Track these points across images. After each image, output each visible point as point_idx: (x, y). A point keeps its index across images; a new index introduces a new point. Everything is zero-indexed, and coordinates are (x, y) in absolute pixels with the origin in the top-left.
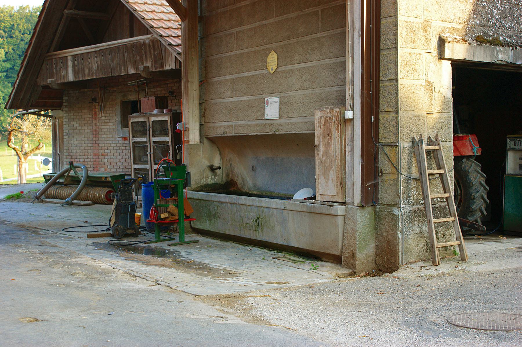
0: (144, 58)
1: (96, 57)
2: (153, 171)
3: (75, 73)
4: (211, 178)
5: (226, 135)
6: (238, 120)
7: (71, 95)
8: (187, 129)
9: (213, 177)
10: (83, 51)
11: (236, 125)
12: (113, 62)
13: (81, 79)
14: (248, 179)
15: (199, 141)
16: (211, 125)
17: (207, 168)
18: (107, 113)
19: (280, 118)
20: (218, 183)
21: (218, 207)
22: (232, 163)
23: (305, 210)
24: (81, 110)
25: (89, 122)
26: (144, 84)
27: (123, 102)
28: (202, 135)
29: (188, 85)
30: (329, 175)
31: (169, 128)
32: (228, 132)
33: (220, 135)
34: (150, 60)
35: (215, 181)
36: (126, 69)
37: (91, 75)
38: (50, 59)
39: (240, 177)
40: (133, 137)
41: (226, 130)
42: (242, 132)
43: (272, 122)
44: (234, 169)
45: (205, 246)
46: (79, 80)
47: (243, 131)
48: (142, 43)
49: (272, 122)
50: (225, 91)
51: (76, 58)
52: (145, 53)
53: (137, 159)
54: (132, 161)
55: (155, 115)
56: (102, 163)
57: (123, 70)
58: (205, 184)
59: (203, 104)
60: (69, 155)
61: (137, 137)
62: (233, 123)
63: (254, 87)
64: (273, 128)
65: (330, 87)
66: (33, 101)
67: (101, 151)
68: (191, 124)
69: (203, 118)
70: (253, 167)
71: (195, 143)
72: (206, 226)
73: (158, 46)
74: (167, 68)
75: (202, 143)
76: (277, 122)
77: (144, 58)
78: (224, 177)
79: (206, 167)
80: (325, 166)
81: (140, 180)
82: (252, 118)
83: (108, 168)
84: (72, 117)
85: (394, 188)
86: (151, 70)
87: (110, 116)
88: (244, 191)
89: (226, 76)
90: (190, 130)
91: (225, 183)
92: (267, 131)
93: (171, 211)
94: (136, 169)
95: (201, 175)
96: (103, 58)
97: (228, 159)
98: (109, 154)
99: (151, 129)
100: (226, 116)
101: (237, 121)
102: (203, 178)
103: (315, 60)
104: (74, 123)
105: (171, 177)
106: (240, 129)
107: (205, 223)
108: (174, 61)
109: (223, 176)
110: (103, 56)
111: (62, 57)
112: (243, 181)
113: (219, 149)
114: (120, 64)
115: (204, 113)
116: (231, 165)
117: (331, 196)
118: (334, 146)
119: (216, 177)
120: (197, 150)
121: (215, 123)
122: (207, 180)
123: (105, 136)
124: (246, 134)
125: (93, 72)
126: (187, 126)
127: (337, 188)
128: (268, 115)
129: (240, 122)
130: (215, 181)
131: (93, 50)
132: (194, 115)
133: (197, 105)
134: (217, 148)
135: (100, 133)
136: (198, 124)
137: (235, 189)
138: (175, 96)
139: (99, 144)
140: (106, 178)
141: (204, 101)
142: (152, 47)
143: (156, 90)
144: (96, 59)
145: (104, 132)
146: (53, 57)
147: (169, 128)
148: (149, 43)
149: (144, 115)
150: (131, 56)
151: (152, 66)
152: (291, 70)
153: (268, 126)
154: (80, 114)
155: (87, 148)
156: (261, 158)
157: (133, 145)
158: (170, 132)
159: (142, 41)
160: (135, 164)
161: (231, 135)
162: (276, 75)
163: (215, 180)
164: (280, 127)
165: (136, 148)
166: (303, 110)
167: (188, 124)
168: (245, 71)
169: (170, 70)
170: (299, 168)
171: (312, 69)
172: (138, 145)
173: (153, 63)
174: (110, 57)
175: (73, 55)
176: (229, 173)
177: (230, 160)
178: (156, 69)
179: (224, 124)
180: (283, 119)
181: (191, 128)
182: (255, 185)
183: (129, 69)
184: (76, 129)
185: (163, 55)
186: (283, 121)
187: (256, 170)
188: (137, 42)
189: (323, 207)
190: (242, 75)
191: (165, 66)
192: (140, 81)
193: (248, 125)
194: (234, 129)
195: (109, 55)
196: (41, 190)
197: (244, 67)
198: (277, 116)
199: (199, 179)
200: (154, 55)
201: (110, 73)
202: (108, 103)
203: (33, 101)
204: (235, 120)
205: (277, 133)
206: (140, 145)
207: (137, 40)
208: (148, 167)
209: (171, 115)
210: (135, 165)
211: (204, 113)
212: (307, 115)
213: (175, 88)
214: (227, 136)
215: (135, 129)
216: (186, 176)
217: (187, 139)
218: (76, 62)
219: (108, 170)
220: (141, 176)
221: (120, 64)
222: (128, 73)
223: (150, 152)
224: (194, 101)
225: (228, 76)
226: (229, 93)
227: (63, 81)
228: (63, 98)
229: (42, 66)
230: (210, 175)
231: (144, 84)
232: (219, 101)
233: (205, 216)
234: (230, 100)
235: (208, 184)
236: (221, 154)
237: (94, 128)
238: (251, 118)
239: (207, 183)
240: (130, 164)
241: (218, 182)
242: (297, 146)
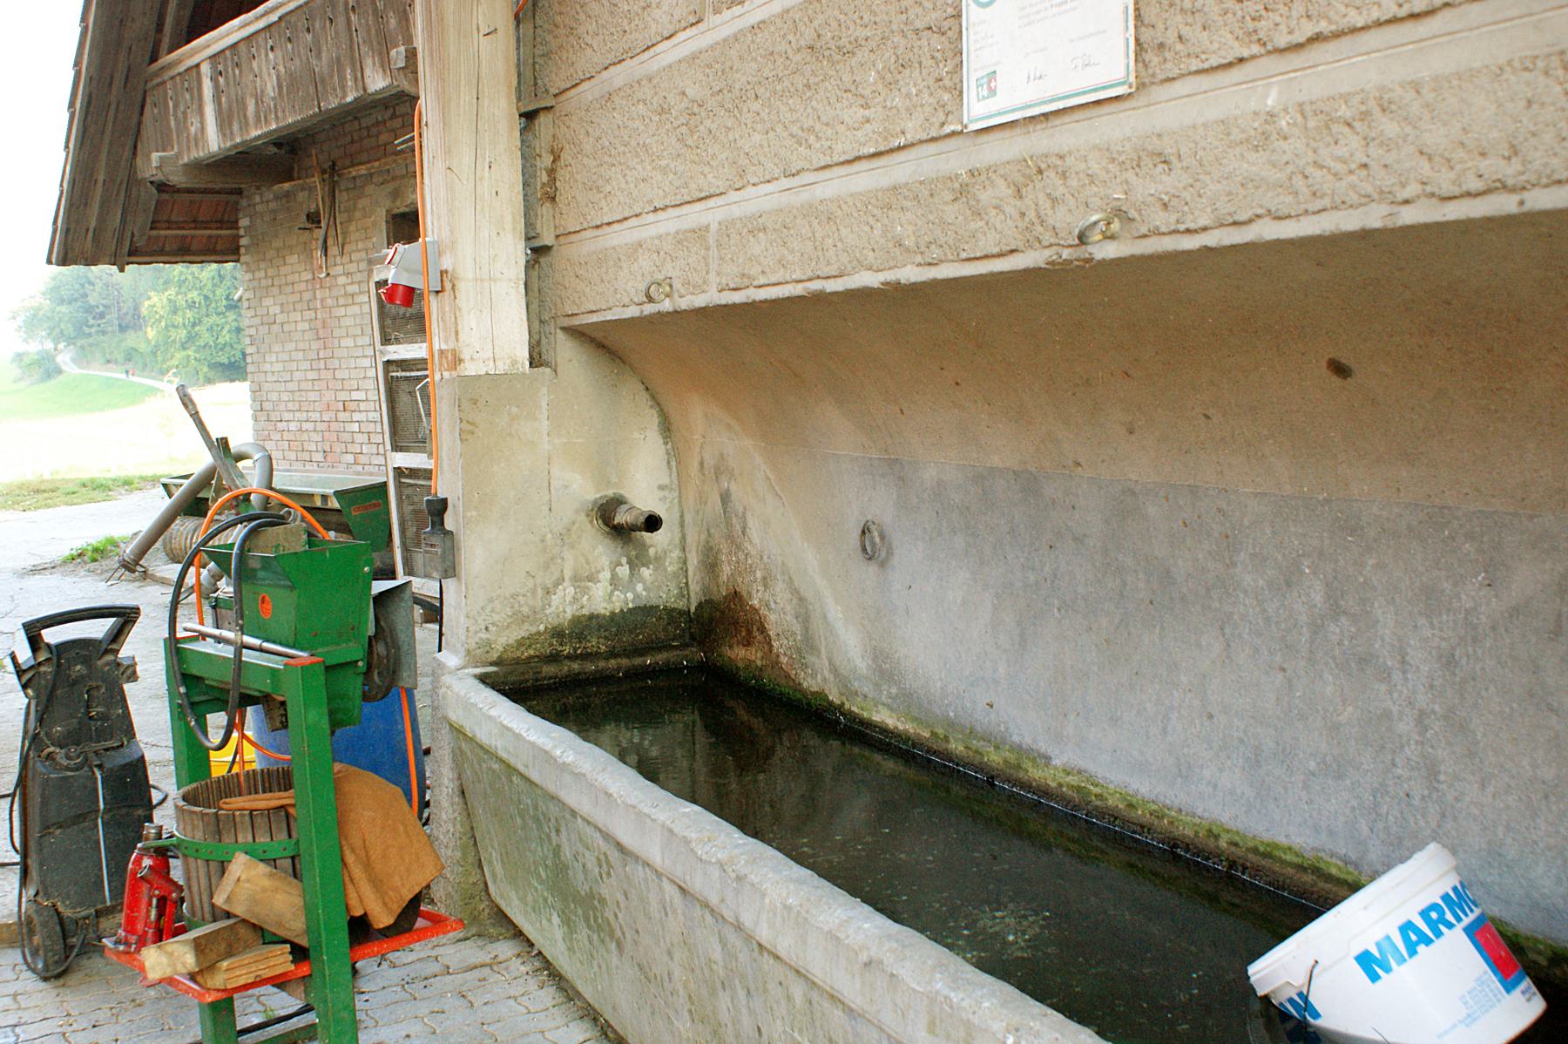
1: (272, 49)
3: (224, 122)
4: (615, 580)
5: (667, 306)
7: (258, 208)
8: (446, 283)
9: (624, 571)
10: (234, 35)
11: (726, 227)
12: (319, 56)
13: (238, 140)
14: (835, 613)
15: (523, 354)
16: (588, 245)
17: (582, 517)
18: (351, 261)
19: (1141, 86)
20: (654, 608)
22: (733, 487)
24: (284, 257)
25: (307, 296)
27: (395, 217)
32: (677, 285)
33: (632, 312)
35: (637, 596)
36: (360, 79)
37: (263, 119)
38: (158, 85)
39: (780, 587)
40: (386, 340)
41: (670, 270)
44: (744, 533)
46: (233, 143)
47: (782, 262)
51: (220, 67)
56: (347, 437)
57: (349, 83)
58: (576, 620)
60: (262, 410)
61: (398, 341)
64: (1054, 201)
66: (133, 234)
67: (343, 396)
69: (545, 210)
70: (865, 531)
71: (501, 368)
75: (547, 365)
76: (1116, 128)
78: (690, 573)
79: (577, 512)
82: (844, 149)
83: (361, 453)
84: (262, 281)
87: (360, 271)
90: (462, 287)
91: (700, 606)
94: (399, 468)
95: (546, 567)
96: (289, 46)
97: (710, 462)
98: (363, 406)
100: (664, 171)
101: (733, 196)
102: (560, 581)
104: (268, 302)
106: (757, 249)
109: (685, 562)
110: (289, 40)
111: (186, 70)
112: (805, 618)
113: (653, 397)
114: (338, 59)
115: (552, 172)
116: (725, 498)
119: (646, 572)
120: (514, 410)
121: (607, 229)
122: (585, 591)
123: (349, 342)
124: (798, 290)
125: (269, 105)
126: (447, 263)
128: (1000, 83)
129: (758, 199)
130: (637, 596)
131: (261, 24)
133: (503, 126)
134: (645, 395)
135: (337, 333)
136: (515, 254)
139: (335, 369)
140: (324, 497)
144: (271, 55)
145: (347, 327)
146: (166, 77)
150: (370, 18)
153: (1004, 190)
154: (284, 270)
155: (304, 386)
156: (929, 474)
157: (386, 372)
160: (397, 448)
161: (700, 301)
163: (639, 588)
164: (1147, 187)
170: (1318, 598)
172: (404, 374)
174: (309, 37)
175: (214, 56)
176: (719, 551)
177: (718, 473)
180: (1179, 88)
182: (885, 668)
183: (368, 72)
184: (275, 323)
187: (890, 554)
194: (714, 252)
195: (308, 30)
196: (142, 534)
199: (534, 592)
201: (313, 100)
202: (352, 228)
203: (133, 234)
204: (721, 185)
205: (1106, 251)
206: (408, 374)
210: (399, 455)
211: (552, 172)
214: (677, 313)
216: (372, 610)
217: (451, 346)
218: (221, 80)
219: (363, 460)
221: (338, 59)
222: (365, 90)
224: (485, 102)
227: (196, 155)
228: (237, 222)
229: (142, 114)
230: (605, 561)
232: (618, 76)
234: (690, 42)
235: (592, 617)
236: (667, 428)
237: (319, 316)
238: (839, 147)
239: (585, 612)
240: (382, 451)
241: (654, 602)
242: (1336, 381)
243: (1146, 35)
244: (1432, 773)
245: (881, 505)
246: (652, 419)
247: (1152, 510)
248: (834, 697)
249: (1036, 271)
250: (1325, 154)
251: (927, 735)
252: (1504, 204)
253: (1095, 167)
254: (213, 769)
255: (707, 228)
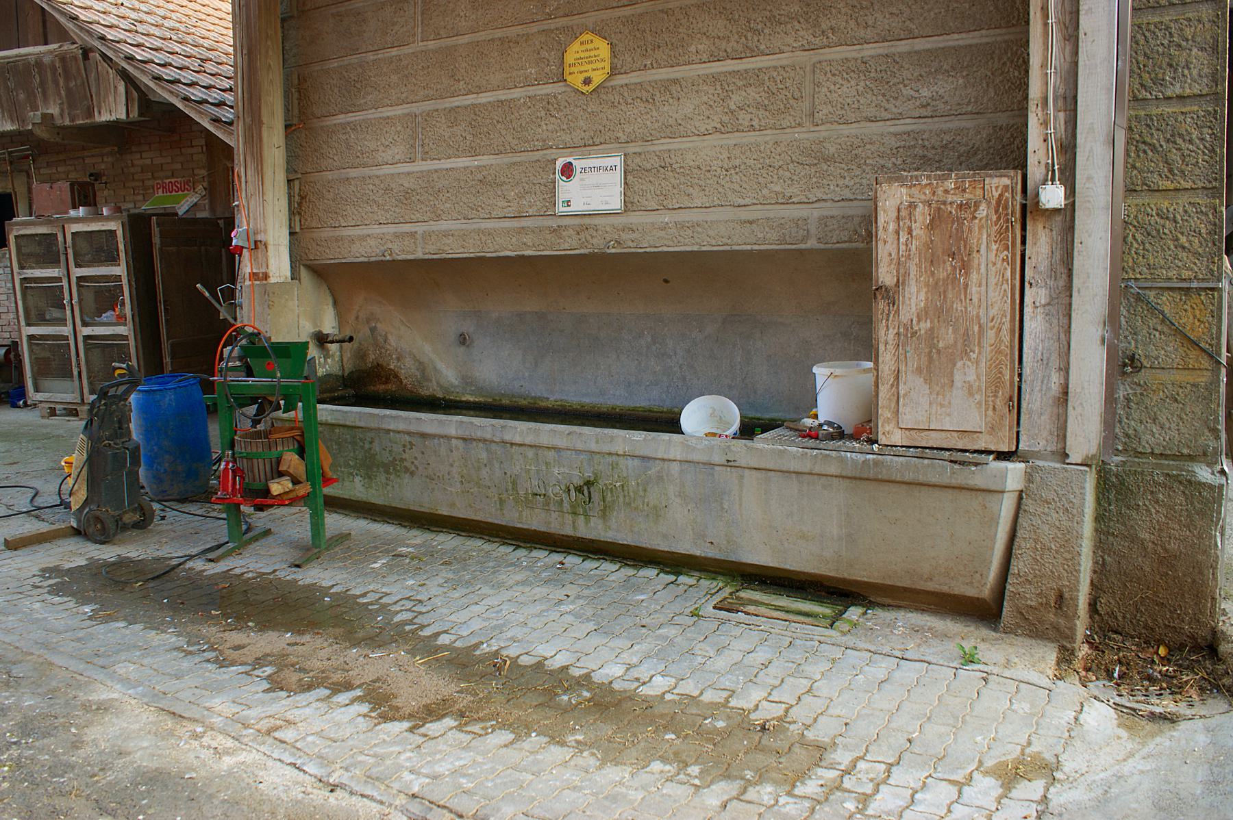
0: (39, 96)
2: (80, 339)
5: (388, 258)
6: (438, 218)
15: (289, 274)
21: (404, 446)
22: (379, 325)
23: (833, 470)
26: (27, 157)
28: (297, 260)
29: (260, 131)
30: (952, 374)
31: (121, 247)
34: (55, 101)
42: (455, 250)
43: (587, 221)
45: (420, 561)
48: (33, 63)
49: (587, 221)
50: (381, 148)
52: (43, 84)
53: (33, 313)
54: (22, 319)
55: (77, 220)
59: (297, 183)
62: (420, 228)
63: (503, 132)
65: (863, 124)
68: (270, 232)
71: (282, 280)
72: (355, 488)
73: (79, 69)
74: (105, 117)
77: (39, 96)
80: (932, 346)
81: (119, 375)
85: (1198, 410)
86: (59, 122)
88: (425, 392)
89: (380, 110)
90: (270, 248)
92: (569, 245)
93: (291, 471)
99: (70, 251)
103: (786, 49)
105: (279, 375)
107: (347, 483)
108: (124, 102)
115: (300, 204)
116: (373, 330)
117: (955, 434)
118: (983, 288)
119: (329, 360)
126: (259, 238)
127: (990, 412)
129: (444, 225)
132: (277, 209)
133: (282, 184)
136: (285, 232)
137: (392, 387)
138: (106, 183)
141: (300, 176)
142: (60, 71)
143: (54, 171)
147: (121, 247)
148: (53, 62)
149: (42, 219)
151: (62, 115)
152: (676, 81)
157: (21, 284)
158: (122, 255)
159: (32, 60)
160: (28, 325)
162: (601, 96)
165: (29, 292)
166: (737, 187)
167: (265, 232)
168: (463, 92)
169: (113, 121)
170: (649, 340)
171: (775, 74)
173: (65, 106)
178: (72, 120)
179: (376, 230)
181: (271, 241)
182: (467, 381)
185: (94, 90)
186: (635, 219)
188: (19, 61)
189: (928, 465)
190: (451, 102)
191: (100, 113)
192: (16, 151)
193: (480, 232)
197: (459, 81)
198: (616, 203)
200: (69, 90)
207: (17, 56)
208: (66, 330)
209: (126, 220)
210: (32, 328)
211: (300, 204)
212: (755, 201)
213: (103, 167)
215: (24, 250)
220: (124, 366)
223: (71, 299)
225: (390, 108)
226: (398, 151)
231: (27, 157)
233: (347, 465)
236: (335, 303)
243: (627, 199)
244: (684, 379)
245: (468, 327)
246: (330, 301)
247: (591, 320)
248: (440, 395)
249: (585, 255)
250: (681, 233)
251: (490, 400)
252: (728, 248)
253: (608, 229)
254: (319, 413)
255: (416, 232)
